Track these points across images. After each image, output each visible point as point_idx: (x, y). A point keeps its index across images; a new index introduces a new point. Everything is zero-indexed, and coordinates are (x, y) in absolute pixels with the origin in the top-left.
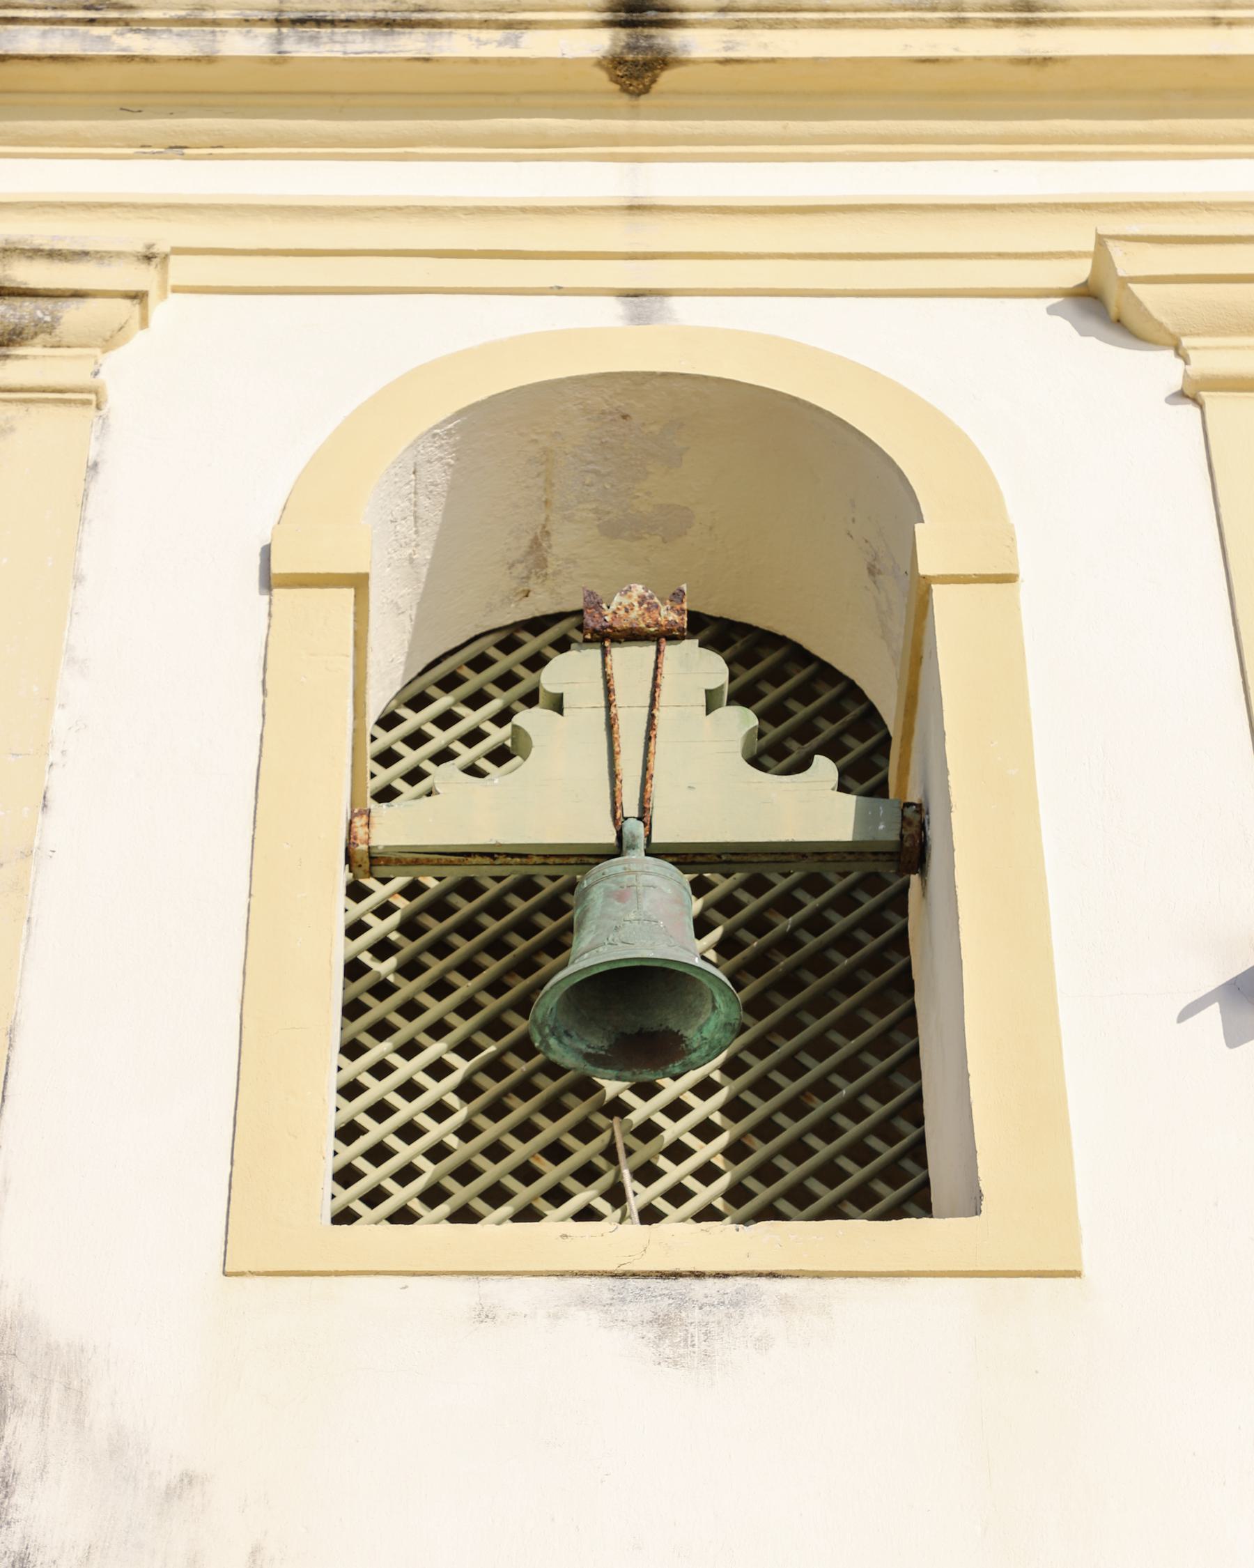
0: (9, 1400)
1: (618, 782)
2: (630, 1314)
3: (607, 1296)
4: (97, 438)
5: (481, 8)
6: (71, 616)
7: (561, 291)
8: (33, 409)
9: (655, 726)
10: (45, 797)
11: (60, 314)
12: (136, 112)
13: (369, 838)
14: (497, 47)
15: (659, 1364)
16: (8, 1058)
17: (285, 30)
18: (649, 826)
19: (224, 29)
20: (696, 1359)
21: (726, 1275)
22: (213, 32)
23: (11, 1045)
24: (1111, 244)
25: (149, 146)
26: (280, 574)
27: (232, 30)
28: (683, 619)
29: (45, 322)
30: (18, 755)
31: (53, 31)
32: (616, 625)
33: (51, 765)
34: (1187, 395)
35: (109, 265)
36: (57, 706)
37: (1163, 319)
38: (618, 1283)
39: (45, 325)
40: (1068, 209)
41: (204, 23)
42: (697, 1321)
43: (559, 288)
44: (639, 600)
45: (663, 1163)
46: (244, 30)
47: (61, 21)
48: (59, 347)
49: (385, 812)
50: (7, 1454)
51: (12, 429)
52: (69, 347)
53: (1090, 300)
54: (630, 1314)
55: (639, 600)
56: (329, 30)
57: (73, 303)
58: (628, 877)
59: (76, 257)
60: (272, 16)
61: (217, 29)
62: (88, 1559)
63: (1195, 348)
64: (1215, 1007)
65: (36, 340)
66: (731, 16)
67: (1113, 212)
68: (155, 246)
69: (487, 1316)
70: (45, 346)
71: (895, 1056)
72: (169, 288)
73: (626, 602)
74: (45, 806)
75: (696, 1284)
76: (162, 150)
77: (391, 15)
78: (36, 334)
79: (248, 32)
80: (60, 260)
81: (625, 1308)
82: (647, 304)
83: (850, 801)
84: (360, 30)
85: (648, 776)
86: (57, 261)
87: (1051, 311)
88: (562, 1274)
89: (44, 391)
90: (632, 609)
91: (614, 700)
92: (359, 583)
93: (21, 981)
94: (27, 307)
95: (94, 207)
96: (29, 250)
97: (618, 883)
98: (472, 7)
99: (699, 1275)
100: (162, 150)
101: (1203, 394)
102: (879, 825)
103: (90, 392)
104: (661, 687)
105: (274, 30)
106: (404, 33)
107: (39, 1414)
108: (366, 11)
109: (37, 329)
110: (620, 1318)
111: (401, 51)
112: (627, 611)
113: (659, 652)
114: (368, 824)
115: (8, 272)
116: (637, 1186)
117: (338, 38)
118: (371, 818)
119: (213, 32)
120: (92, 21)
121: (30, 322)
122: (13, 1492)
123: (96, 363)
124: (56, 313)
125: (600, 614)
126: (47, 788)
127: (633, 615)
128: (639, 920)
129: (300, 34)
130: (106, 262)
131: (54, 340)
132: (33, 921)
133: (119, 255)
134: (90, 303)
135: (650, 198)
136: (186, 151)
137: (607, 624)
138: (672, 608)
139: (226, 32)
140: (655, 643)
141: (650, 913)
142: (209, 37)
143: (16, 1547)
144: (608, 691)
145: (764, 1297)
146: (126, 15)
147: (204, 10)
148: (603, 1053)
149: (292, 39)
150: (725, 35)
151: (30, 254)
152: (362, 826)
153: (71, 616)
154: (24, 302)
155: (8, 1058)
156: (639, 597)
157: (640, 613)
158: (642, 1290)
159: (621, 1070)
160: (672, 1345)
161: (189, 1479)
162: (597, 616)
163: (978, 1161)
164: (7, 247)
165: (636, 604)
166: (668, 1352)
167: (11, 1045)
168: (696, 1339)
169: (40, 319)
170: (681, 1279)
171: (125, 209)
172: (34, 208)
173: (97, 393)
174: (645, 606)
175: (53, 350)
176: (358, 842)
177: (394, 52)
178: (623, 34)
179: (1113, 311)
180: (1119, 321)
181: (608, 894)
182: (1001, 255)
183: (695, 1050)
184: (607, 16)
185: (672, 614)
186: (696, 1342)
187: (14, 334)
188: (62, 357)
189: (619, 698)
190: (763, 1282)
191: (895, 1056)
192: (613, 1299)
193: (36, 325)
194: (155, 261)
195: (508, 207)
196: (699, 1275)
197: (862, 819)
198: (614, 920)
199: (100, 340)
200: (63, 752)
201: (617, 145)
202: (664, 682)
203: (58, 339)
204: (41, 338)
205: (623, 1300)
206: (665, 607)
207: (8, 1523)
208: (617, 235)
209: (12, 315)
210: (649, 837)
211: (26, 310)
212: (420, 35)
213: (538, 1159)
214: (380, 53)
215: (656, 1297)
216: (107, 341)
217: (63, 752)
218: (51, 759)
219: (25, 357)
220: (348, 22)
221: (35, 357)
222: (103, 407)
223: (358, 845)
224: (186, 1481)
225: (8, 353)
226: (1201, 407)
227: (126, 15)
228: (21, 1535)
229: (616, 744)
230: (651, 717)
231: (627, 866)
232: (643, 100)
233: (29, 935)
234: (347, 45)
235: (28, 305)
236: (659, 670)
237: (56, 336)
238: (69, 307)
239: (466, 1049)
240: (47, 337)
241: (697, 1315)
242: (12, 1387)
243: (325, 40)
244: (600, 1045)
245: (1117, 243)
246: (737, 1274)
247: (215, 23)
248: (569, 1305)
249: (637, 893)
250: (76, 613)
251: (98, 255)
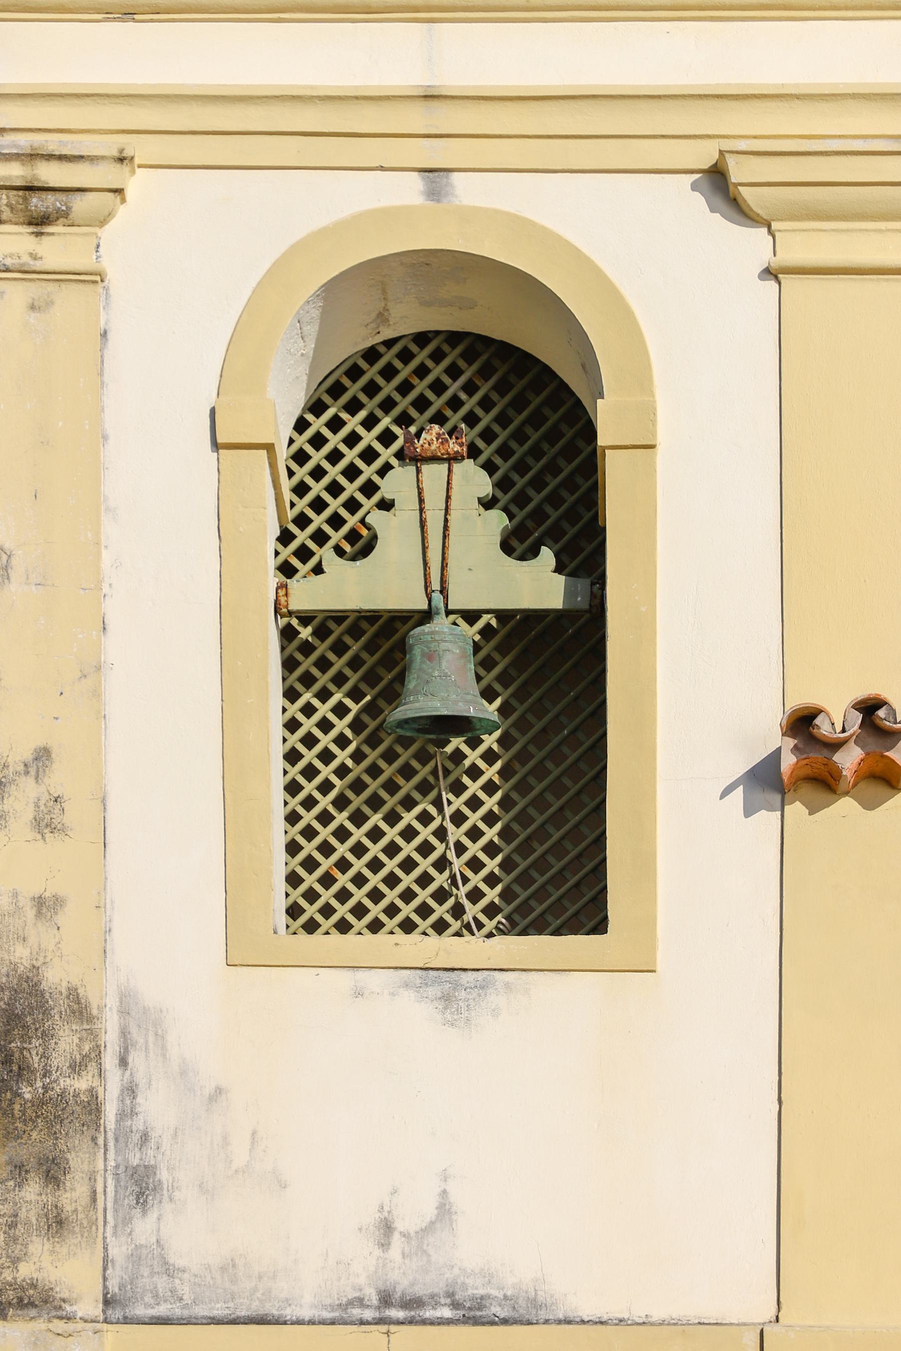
0: (129, 1041)
1: (428, 569)
2: (430, 993)
3: (418, 981)
4: (104, 308)
6: (104, 470)
7: (383, 169)
8: (63, 285)
9: (449, 527)
10: (104, 622)
11: (71, 205)
13: (288, 604)
15: (444, 1025)
16: (104, 817)
18: (446, 598)
20: (463, 1022)
21: (478, 970)
23: (105, 808)
24: (727, 155)
25: (112, 13)
26: (222, 443)
28: (463, 450)
29: (63, 210)
30: (85, 589)
32: (423, 455)
33: (105, 596)
35: (97, 164)
36: (103, 547)
38: (424, 973)
39: (62, 213)
40: (708, 98)
42: (463, 998)
43: (382, 167)
44: (437, 436)
45: (466, 780)
48: (73, 226)
49: (295, 585)
50: (131, 1073)
52: (79, 226)
53: (719, 174)
54: (430, 993)
55: (437, 436)
57: (78, 196)
58: (434, 644)
59: (76, 160)
62: (176, 1136)
63: (779, 231)
64: (740, 790)
65: (58, 222)
67: (737, 99)
68: (125, 151)
69: (359, 994)
70: (64, 225)
71: (549, 902)
72: (136, 166)
73: (429, 438)
74: (104, 629)
75: (463, 975)
76: (120, 16)
78: (58, 218)
80: (66, 161)
81: (428, 989)
82: (438, 180)
83: (561, 579)
85: (445, 565)
86: (64, 162)
88: (396, 968)
90: (432, 443)
91: (424, 507)
92: (270, 448)
93: (105, 762)
94: (50, 199)
95: (82, 96)
96: (46, 155)
97: (428, 648)
99: (465, 970)
100: (120, 16)
102: (578, 597)
104: (452, 498)
107: (144, 1049)
109: (58, 215)
110: (425, 996)
112: (429, 444)
113: (450, 471)
114: (286, 595)
115: (35, 172)
116: (451, 797)
118: (288, 590)
121: (53, 211)
122: (137, 1096)
123: (97, 237)
124: (68, 203)
125: (414, 447)
126: (104, 614)
127: (433, 447)
128: (440, 676)
130: (95, 162)
131: (70, 222)
132: (107, 717)
133: (103, 158)
135: (439, 87)
136: (135, 16)
137: (418, 454)
138: (456, 442)
140: (448, 462)
141: (447, 671)
143: (141, 1128)
144: (421, 501)
145: (497, 983)
148: (428, 727)
151: (47, 158)
152: (283, 596)
153: (104, 470)
154: (47, 195)
155: (104, 817)
156: (437, 434)
157: (438, 445)
158: (436, 978)
159: (439, 734)
160: (452, 1013)
161: (219, 1091)
162: (412, 448)
163: (608, 898)
165: (435, 439)
166: (449, 1017)
167: (105, 808)
168: (463, 1009)
169: (59, 208)
170: (455, 971)
171: (102, 98)
172: (44, 97)
173: (100, 275)
174: (440, 440)
175: (69, 228)
176: (281, 607)
179: (731, 195)
180: (735, 199)
181: (423, 655)
182: (663, 137)
183: (478, 730)
185: (456, 446)
186: (463, 1012)
187: (45, 218)
188: (76, 234)
189: (427, 505)
190: (497, 973)
191: (549, 902)
192: (421, 983)
193: (57, 213)
194: (126, 162)
195: (346, 96)
196: (465, 970)
197: (569, 593)
198: (427, 674)
199: (98, 222)
200: (110, 585)
201: (418, 12)
202: (454, 493)
203: (72, 221)
204: (62, 220)
205: (426, 984)
206: (452, 441)
207: (137, 1114)
209: (41, 205)
210: (446, 605)
213: (396, 777)
215: (442, 982)
216: (102, 222)
217: (110, 585)
218: (104, 591)
219: (53, 234)
221: (59, 234)
222: (105, 279)
223: (281, 609)
224: (218, 1091)
225: (42, 231)
226: (780, 284)
228: (143, 1121)
229: (426, 541)
230: (446, 521)
231: (433, 636)
233: (106, 728)
235: (50, 197)
236: (450, 485)
237: (70, 219)
239: (357, 695)
240: (65, 220)
241: (463, 994)
242: (129, 1033)
244: (426, 722)
245: (731, 155)
246: (483, 969)
248: (399, 987)
249: (439, 655)
250: (107, 468)
251: (90, 158)
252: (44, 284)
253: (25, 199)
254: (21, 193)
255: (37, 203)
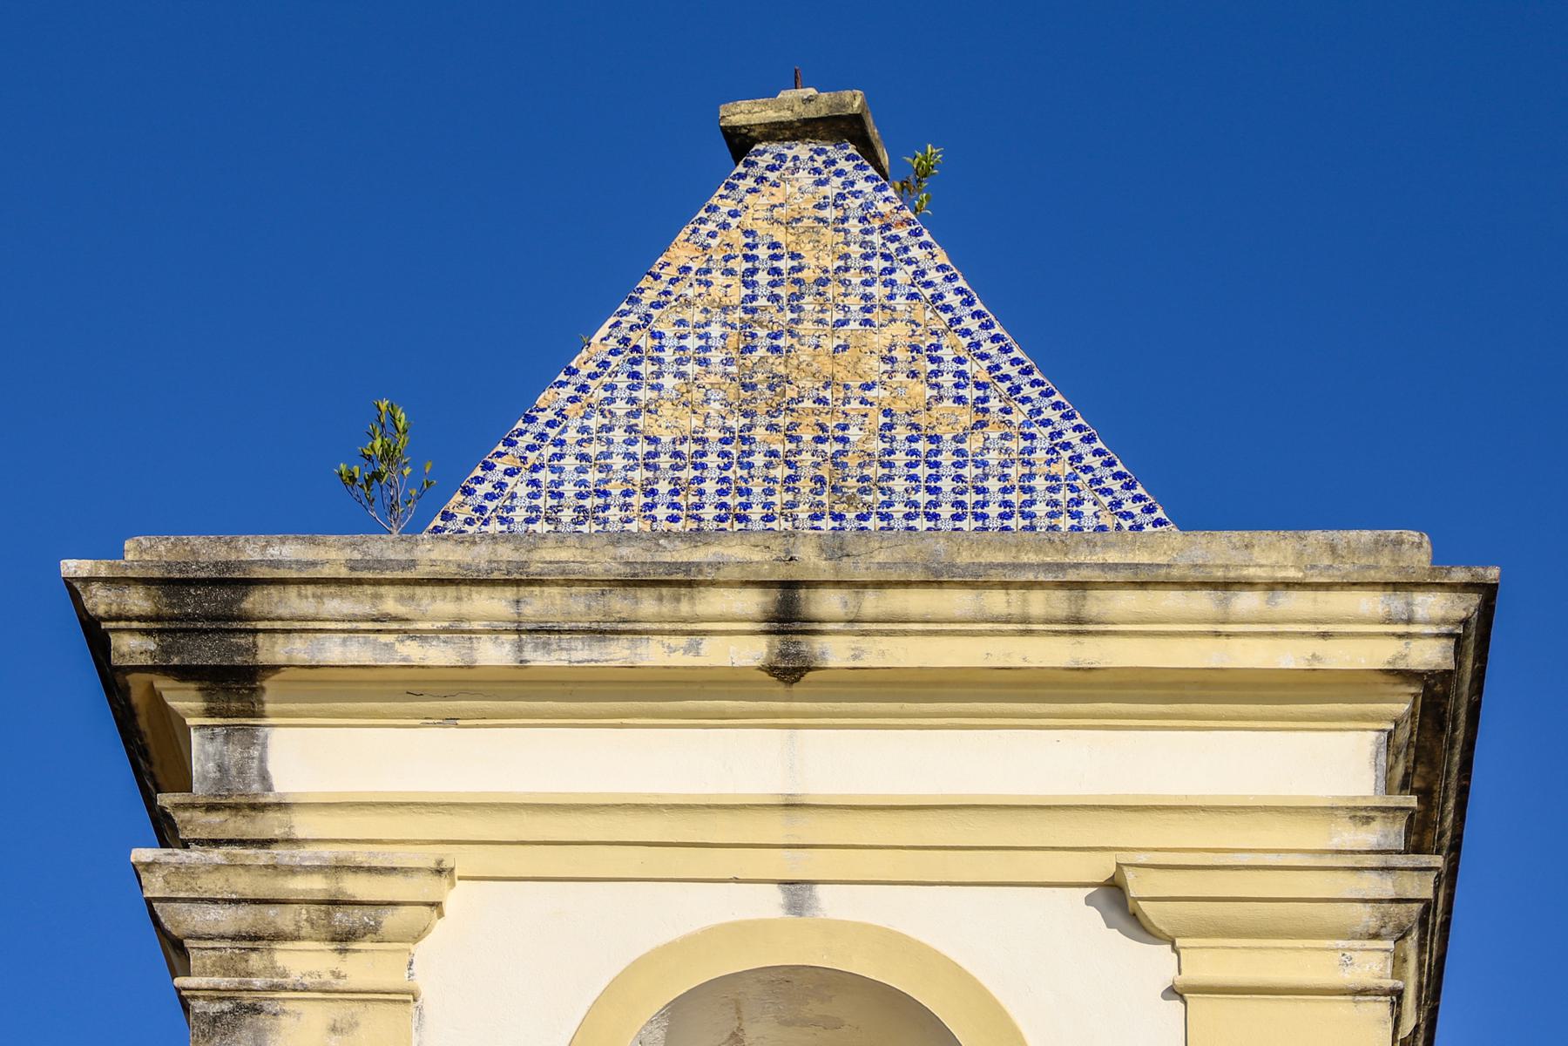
4: (417, 1029)
5: (670, 620)
8: (370, 1005)
12: (418, 695)
14: (684, 654)
17: (524, 636)
19: (478, 636)
22: (470, 638)
24: (1125, 868)
27: (484, 637)
29: (371, 926)
31: (351, 638)
34: (1174, 993)
37: (1162, 928)
41: (463, 632)
43: (737, 879)
46: (494, 636)
47: (357, 631)
51: (357, 1024)
56: (557, 637)
57: (389, 910)
60: (513, 626)
61: (473, 636)
65: (365, 938)
66: (857, 627)
76: (441, 721)
77: (603, 626)
79: (497, 638)
84: (580, 636)
87: (1089, 901)
89: (376, 993)
98: (662, 619)
100: (441, 721)
101: (1186, 995)
103: (408, 994)
105: (516, 636)
106: (613, 639)
108: (583, 622)
111: (612, 660)
117: (564, 645)
119: (470, 638)
120: (379, 631)
129: (535, 641)
130: (409, 874)
131: (379, 938)
133: (418, 869)
134: (403, 910)
136: (458, 722)
139: (480, 638)
142: (468, 644)
146: (405, 626)
147: (462, 621)
149: (530, 646)
150: (854, 642)
154: (355, 909)
164: (337, 865)
169: (367, 923)
173: (413, 994)
177: (607, 661)
178: (777, 639)
180: (1134, 915)
182: (1053, 849)
184: (763, 626)
187: (350, 934)
208: (776, 828)
211: (356, 916)
212: (625, 640)
214: (596, 661)
219: (359, 951)
220: (570, 631)
226: (1186, 1003)
227: (405, 626)
232: (796, 688)
234: (572, 652)
235: (357, 912)
238: (386, 913)
243: (554, 647)
245: (1131, 869)
247: (471, 631)
252: (348, 1004)
253: (328, 914)
254: (323, 907)
255: (341, 917)
